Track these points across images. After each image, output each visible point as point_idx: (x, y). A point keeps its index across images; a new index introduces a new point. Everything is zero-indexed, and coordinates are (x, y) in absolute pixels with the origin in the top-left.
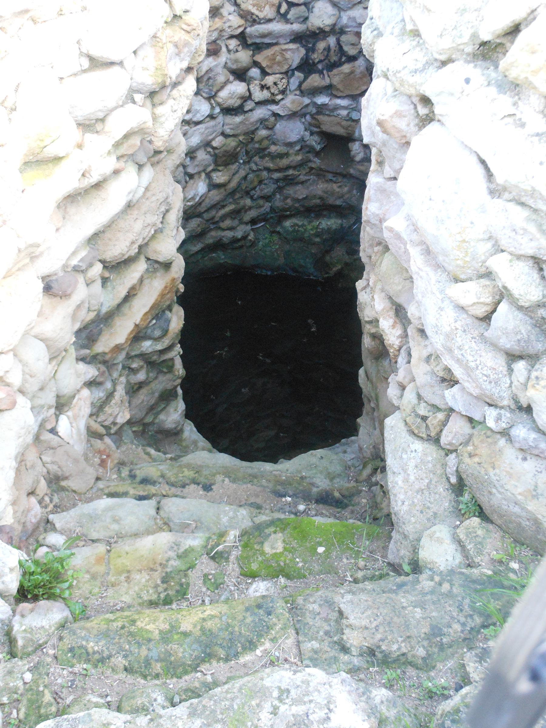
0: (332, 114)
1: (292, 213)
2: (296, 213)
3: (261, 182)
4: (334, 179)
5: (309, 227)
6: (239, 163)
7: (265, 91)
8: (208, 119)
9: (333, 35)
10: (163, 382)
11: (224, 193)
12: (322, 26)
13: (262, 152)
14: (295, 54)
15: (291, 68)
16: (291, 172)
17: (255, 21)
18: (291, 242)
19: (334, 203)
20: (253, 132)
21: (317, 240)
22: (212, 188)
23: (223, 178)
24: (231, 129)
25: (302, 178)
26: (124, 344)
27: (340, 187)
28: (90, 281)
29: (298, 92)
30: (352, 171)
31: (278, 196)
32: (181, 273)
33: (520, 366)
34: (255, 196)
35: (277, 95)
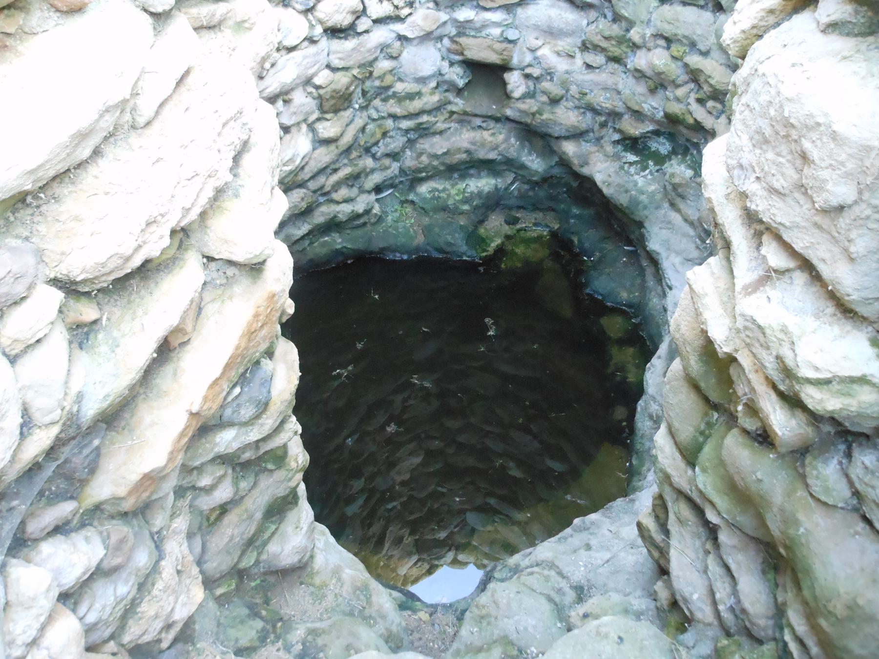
0: (478, 35)
1: (430, 174)
2: (433, 174)
3: (384, 134)
4: (484, 125)
5: (453, 192)
6: (354, 109)
8: (306, 43)
10: (269, 487)
11: (336, 152)
13: (384, 92)
16: (425, 118)
18: (431, 214)
20: (371, 63)
21: (466, 207)
22: (318, 144)
23: (332, 130)
24: (340, 59)
25: (440, 126)
26: (166, 465)
27: (493, 134)
28: (20, 347)
30: (509, 112)
31: (408, 153)
32: (287, 280)
34: (379, 154)
35: (403, 8)
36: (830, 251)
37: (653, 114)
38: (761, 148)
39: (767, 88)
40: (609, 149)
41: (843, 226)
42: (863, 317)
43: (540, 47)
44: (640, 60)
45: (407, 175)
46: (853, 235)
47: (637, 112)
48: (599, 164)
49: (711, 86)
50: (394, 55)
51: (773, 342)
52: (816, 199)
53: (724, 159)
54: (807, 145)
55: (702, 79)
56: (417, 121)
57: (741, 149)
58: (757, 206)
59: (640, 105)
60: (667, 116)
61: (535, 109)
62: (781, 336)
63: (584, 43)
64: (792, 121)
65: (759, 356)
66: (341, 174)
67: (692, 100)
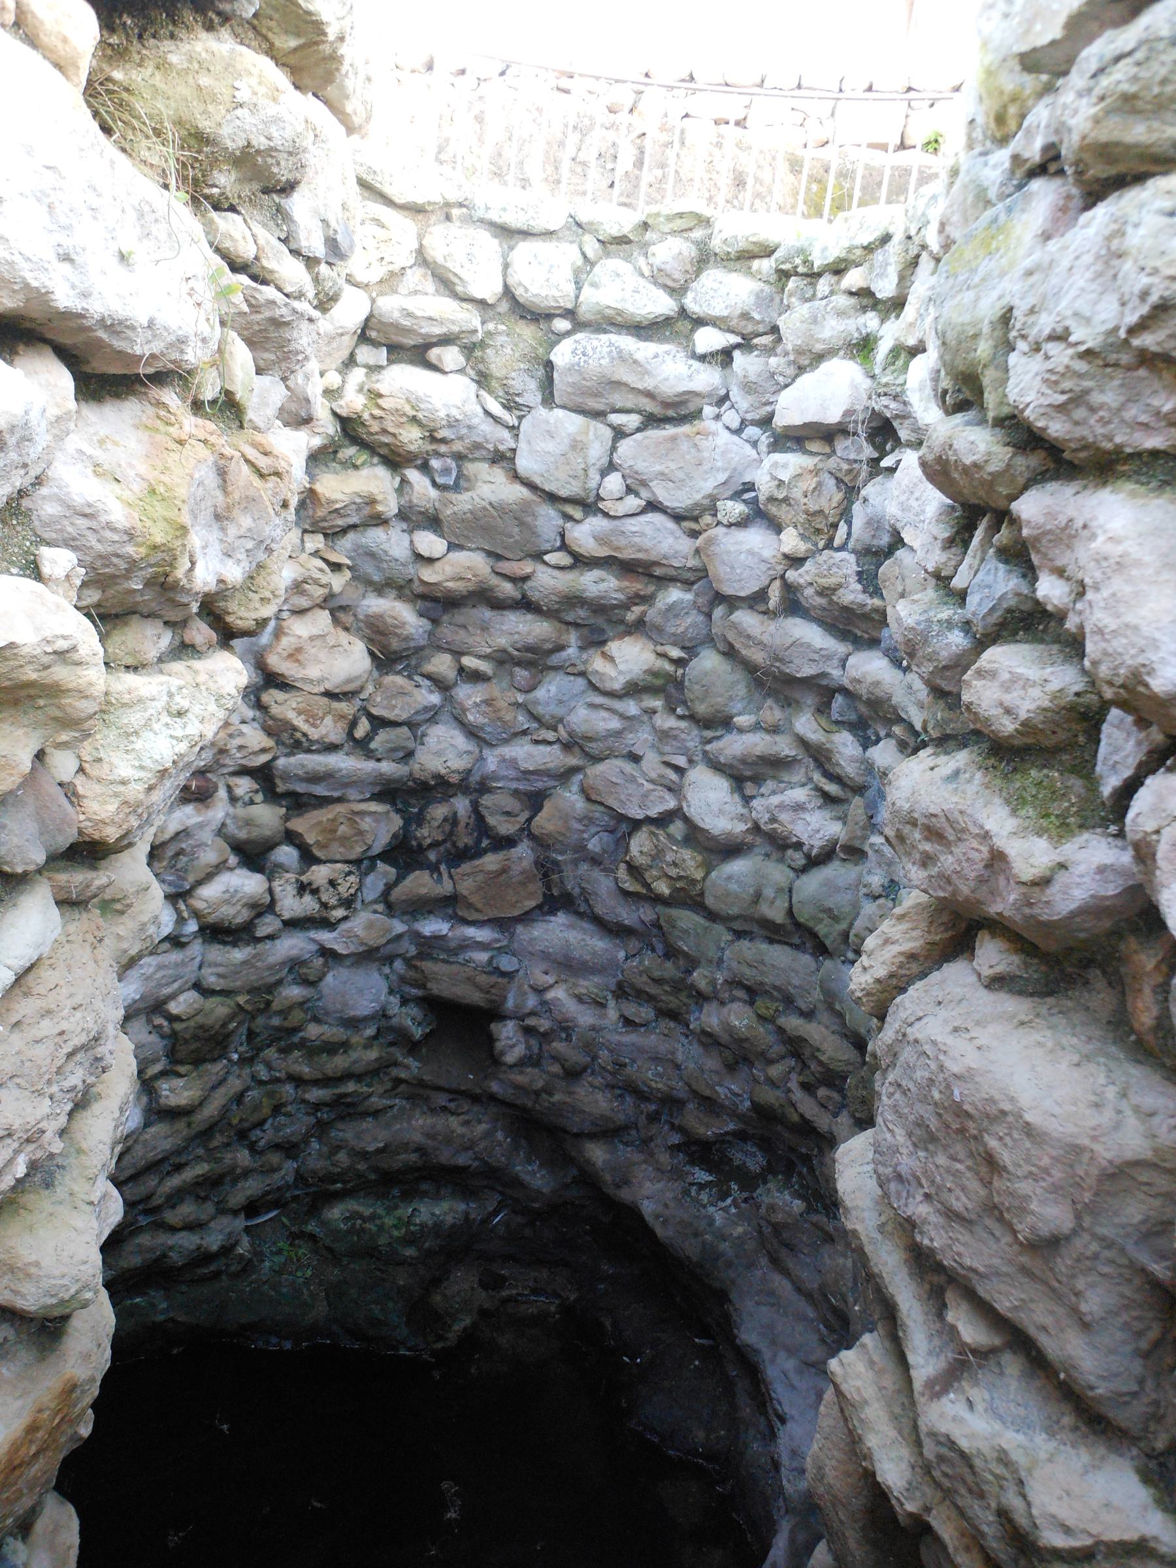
1: (349, 1186)
2: (354, 1186)
3: (277, 1109)
4: (452, 1105)
5: (389, 1221)
6: (230, 1060)
7: (308, 898)
9: (464, 793)
12: (443, 772)
13: (286, 1038)
14: (381, 826)
15: (370, 854)
16: (351, 1087)
17: (298, 745)
19: (452, 1162)
20: (271, 988)
21: (410, 1252)
23: (186, 1094)
24: (219, 975)
25: (376, 1102)
27: (466, 1123)
29: (380, 907)
30: (495, 1087)
31: (315, 1145)
33: (958, 583)
34: (262, 1143)
35: (334, 907)
36: (1052, 1313)
37: (735, 1103)
38: (926, 1150)
39: (923, 1060)
40: (664, 1158)
41: (1063, 1269)
42: (1120, 1430)
43: (551, 986)
44: (710, 1018)
45: (308, 1186)
46: (1080, 1284)
47: (708, 1098)
48: (648, 1184)
49: (821, 1063)
50: (311, 978)
51: (988, 1482)
52: (1019, 1227)
53: (870, 1167)
54: (993, 1143)
55: (807, 1052)
56: (337, 1091)
57: (895, 1150)
58: (932, 1240)
59: (712, 1088)
60: (756, 1107)
61: (540, 1084)
62: (1000, 1470)
63: (620, 985)
64: (966, 1107)
65: (970, 1514)
66: (188, 1175)
67: (793, 1085)
